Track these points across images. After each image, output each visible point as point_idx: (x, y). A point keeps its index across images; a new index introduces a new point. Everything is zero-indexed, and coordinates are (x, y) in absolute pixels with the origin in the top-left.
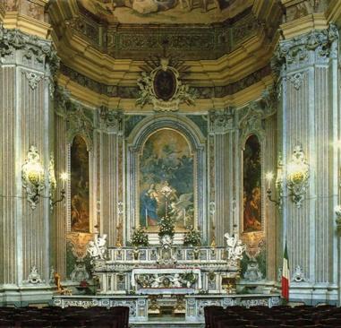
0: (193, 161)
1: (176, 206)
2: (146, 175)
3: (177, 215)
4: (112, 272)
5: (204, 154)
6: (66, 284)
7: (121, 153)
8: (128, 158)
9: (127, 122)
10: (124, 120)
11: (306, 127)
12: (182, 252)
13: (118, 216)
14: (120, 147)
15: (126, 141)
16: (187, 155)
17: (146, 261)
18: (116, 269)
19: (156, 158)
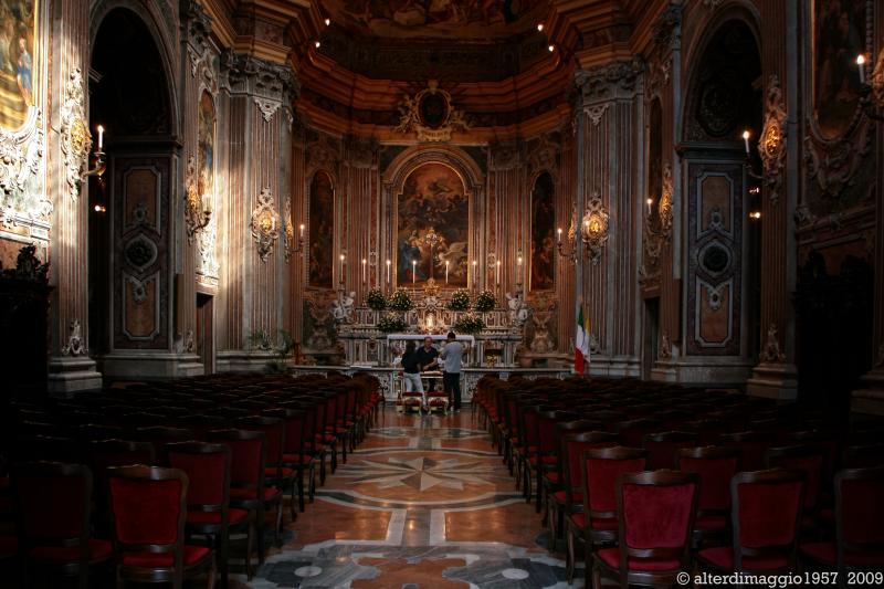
4: (360, 338)
5: (482, 194)
8: (384, 198)
9: (383, 154)
14: (374, 184)
15: (381, 178)
18: (366, 336)
19: (421, 198)
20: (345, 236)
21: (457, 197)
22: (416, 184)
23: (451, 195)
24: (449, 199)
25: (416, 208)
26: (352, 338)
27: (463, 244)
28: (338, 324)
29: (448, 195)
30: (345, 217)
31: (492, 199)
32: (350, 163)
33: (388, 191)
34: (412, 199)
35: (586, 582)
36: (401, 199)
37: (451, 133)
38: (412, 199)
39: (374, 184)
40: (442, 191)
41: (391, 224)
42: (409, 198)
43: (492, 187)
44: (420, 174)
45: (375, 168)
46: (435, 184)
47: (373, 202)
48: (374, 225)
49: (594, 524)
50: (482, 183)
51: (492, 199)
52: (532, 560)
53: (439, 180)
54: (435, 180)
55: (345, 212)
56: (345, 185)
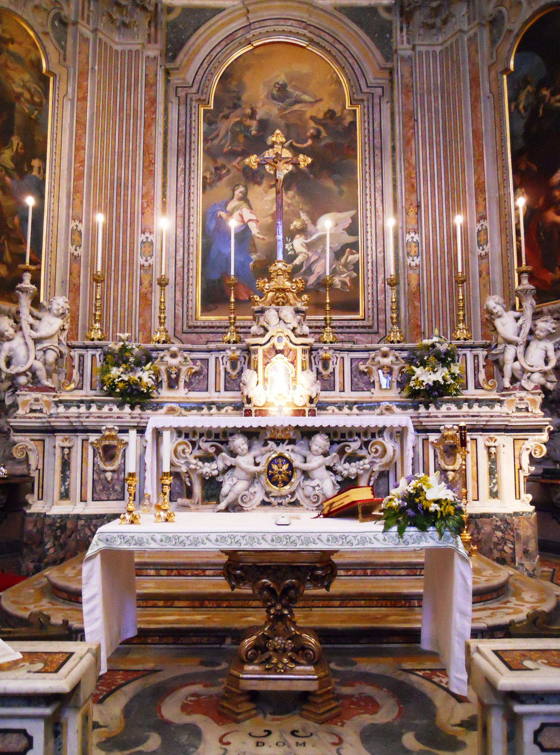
0: (353, 123)
1: (309, 246)
2: (221, 161)
3: (309, 271)
4: (75, 431)
5: (386, 108)
6: (290, 27)
7: (153, 101)
8: (173, 116)
9: (172, 25)
10: (164, 18)
11: (331, 235)
12: (335, 366)
13: (138, 272)
14: (150, 86)
15: (167, 72)
16: (338, 110)
17: (211, 396)
18: (89, 423)
19: (252, 116)
20: (77, 190)
21: (331, 114)
22: (241, 86)
23: (319, 110)
24: (312, 118)
25: (241, 139)
26: (52, 431)
27: (352, 213)
28: (14, 388)
29: (310, 112)
30: (79, 148)
31: (410, 116)
32: (95, 31)
33: (185, 102)
34: (234, 119)
35: (310, 289)
36: (210, 120)
37: (543, 388)
38: (234, 119)
39: (150, 86)
40: (298, 101)
41: (187, 171)
42: (226, 117)
43: (408, 90)
44: (248, 67)
45: (153, 51)
46: (282, 88)
47: (149, 124)
48: (149, 172)
49: (250, 8)
50: (385, 82)
51: (410, 116)
52: (366, 716)
53: (291, 78)
54: (282, 79)
55: (79, 137)
56: (83, 75)
